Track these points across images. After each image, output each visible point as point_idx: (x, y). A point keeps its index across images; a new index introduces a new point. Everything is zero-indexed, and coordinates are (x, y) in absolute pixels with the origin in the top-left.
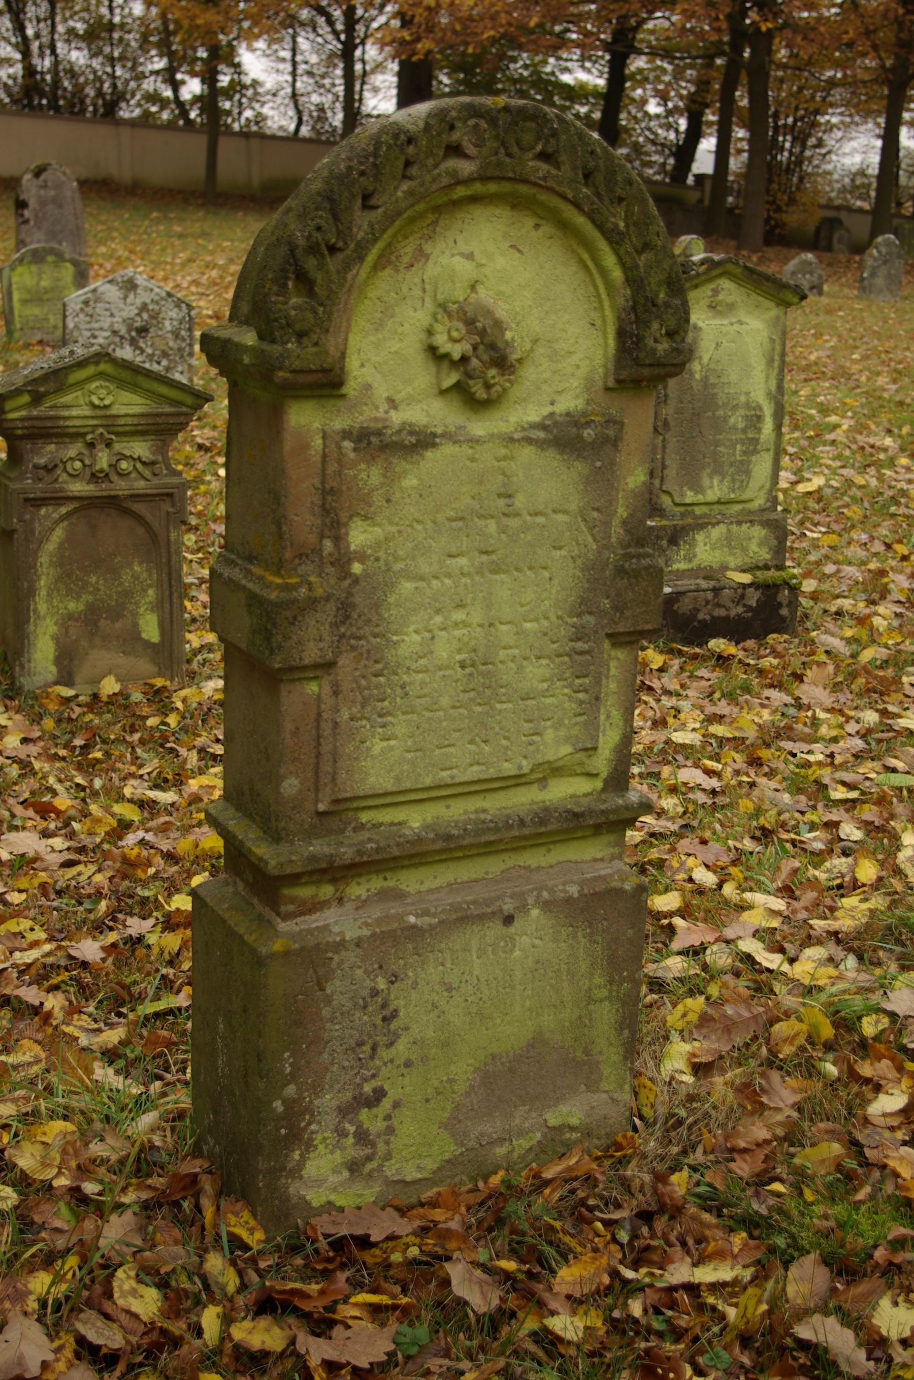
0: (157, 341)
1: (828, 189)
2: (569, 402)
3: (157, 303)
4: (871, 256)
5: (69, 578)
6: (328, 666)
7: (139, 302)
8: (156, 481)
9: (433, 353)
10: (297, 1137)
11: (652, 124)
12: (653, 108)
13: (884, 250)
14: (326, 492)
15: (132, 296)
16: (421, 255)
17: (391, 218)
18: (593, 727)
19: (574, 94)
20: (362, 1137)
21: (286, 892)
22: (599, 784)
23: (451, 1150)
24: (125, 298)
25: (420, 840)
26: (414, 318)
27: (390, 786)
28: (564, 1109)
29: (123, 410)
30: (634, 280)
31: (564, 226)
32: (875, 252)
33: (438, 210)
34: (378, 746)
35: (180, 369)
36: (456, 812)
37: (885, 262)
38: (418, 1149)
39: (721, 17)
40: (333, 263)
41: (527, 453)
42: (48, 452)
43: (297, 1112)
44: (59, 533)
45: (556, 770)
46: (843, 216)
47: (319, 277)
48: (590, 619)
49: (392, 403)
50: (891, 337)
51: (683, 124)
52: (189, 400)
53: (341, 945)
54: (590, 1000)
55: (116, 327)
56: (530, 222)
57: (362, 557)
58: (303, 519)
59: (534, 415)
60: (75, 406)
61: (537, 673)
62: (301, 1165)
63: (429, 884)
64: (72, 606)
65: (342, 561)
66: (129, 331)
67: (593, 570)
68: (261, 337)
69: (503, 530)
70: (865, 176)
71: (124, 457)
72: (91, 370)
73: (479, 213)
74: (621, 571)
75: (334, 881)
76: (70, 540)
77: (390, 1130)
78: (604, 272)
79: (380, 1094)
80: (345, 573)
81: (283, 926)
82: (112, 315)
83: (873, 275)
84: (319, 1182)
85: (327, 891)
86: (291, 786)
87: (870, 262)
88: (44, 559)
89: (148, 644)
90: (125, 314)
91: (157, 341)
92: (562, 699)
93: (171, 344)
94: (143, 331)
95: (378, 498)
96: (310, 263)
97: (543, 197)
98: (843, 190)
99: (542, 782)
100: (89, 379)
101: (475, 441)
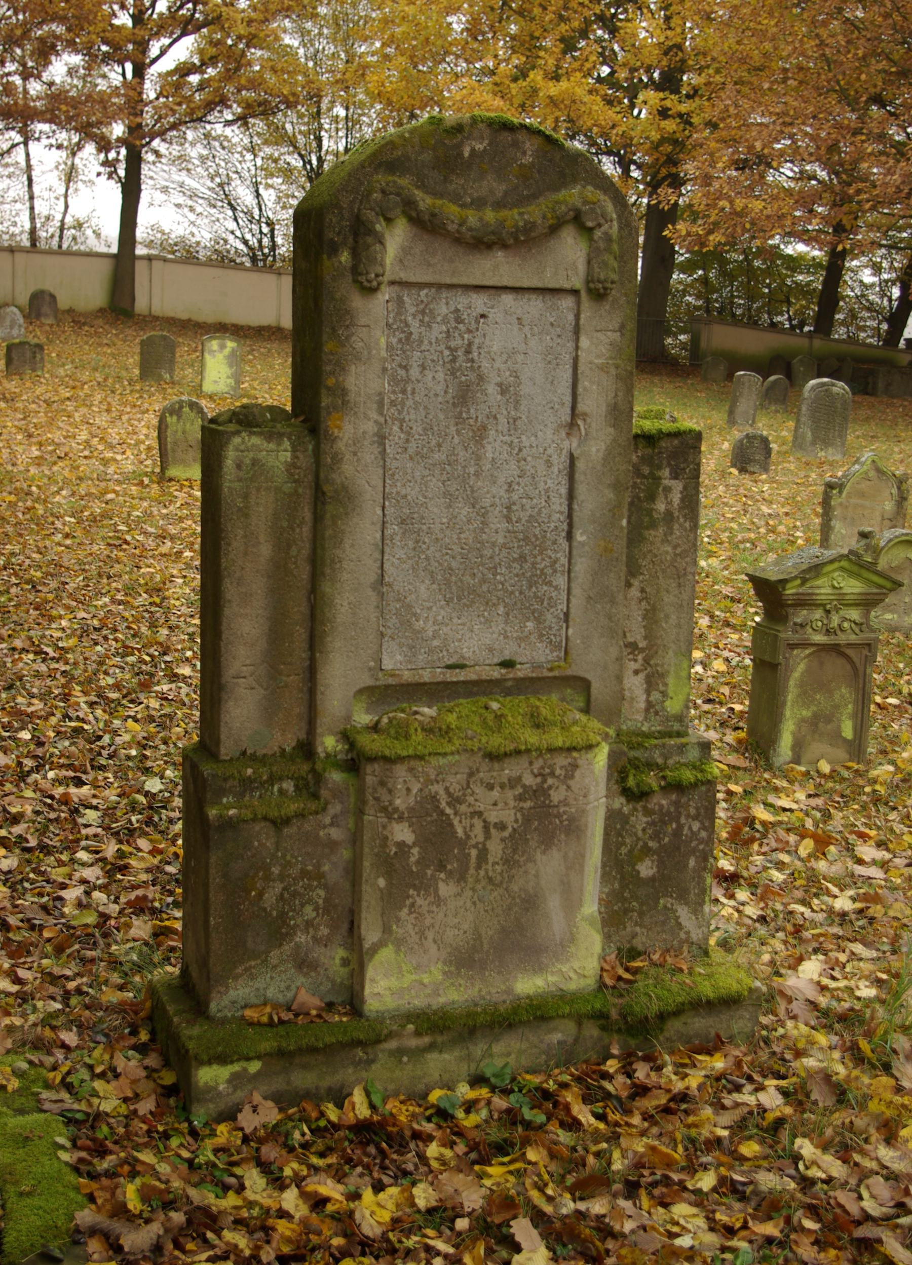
5: (805, 696)
8: (862, 635)
12: (867, 277)
19: (794, 263)
29: (850, 590)
42: (801, 615)
44: (801, 667)
52: (888, 585)
60: (822, 588)
64: (804, 713)
71: (846, 619)
72: (836, 565)
76: (808, 671)
88: (792, 683)
89: (845, 740)
100: (834, 571)
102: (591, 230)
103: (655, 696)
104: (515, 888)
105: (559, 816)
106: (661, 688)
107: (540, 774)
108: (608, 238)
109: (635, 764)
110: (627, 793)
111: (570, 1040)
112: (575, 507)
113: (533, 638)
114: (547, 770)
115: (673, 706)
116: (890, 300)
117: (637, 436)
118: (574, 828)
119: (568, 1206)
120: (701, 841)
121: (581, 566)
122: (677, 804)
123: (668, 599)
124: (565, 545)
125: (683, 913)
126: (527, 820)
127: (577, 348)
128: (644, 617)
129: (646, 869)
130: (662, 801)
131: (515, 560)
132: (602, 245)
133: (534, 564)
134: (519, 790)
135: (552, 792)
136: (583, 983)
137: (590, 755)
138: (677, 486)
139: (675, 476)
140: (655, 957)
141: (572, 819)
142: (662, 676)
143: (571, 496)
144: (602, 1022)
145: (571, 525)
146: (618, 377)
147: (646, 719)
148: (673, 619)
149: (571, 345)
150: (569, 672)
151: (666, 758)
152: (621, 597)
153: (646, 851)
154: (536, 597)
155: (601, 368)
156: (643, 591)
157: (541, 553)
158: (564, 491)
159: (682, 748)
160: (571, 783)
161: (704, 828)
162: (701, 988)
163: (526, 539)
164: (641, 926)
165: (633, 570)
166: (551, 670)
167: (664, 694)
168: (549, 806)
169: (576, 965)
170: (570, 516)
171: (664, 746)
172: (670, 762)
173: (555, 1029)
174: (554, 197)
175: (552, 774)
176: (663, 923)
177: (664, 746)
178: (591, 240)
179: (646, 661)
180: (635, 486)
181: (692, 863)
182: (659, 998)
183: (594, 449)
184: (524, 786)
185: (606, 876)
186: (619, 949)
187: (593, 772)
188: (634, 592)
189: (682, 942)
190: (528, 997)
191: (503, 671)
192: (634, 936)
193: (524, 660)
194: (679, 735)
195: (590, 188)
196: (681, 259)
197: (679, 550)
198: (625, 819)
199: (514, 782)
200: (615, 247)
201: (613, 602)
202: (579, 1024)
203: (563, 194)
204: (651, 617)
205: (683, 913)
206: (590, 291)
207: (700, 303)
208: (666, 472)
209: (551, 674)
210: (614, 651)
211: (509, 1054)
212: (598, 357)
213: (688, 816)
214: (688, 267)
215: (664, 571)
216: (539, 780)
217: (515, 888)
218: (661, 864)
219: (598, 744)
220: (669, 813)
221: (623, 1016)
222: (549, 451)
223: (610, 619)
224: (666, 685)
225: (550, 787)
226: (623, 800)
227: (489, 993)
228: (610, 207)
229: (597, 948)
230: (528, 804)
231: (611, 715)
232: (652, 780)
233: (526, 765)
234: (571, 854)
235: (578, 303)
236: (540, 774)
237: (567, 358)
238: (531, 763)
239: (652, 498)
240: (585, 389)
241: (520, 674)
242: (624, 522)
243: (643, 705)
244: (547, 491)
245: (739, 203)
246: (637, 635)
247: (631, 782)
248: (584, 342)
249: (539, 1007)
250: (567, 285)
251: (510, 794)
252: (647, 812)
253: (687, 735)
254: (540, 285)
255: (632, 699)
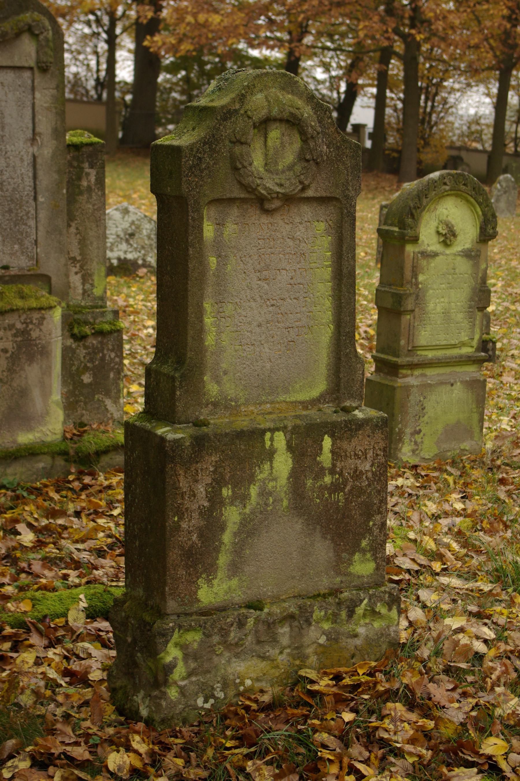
0: (139, 240)
1: (450, 134)
2: (468, 246)
3: (139, 220)
4: (496, 188)
6: (413, 311)
7: (130, 220)
9: (438, 233)
10: (400, 440)
11: (319, 87)
12: (320, 74)
13: (504, 185)
14: (413, 267)
15: (126, 217)
16: (435, 209)
17: (431, 200)
18: (473, 332)
20: (416, 443)
21: (401, 371)
22: (474, 350)
23: (437, 451)
24: (123, 218)
25: (432, 359)
26: (433, 224)
27: (425, 344)
28: (465, 444)
30: (484, 214)
31: (468, 201)
32: (498, 186)
33: (440, 198)
34: (423, 333)
35: (150, 255)
36: (440, 354)
37: (505, 192)
38: (429, 450)
39: (390, 30)
40: (419, 211)
41: (459, 258)
43: (401, 432)
45: (463, 344)
46: (463, 154)
47: (415, 214)
48: (473, 303)
49: (428, 245)
50: (514, 240)
51: (343, 87)
53: (413, 386)
54: (472, 412)
55: (119, 233)
56: (459, 200)
57: (421, 283)
58: (408, 273)
59: (460, 248)
61: (460, 316)
62: (401, 449)
63: (433, 373)
65: (417, 284)
66: (125, 235)
67: (474, 289)
68: (400, 228)
69: (453, 278)
70: (478, 124)
73: (449, 198)
74: (480, 291)
75: (411, 369)
77: (422, 442)
78: (477, 213)
79: (420, 431)
80: (417, 287)
81: (399, 380)
82: (117, 227)
83: (498, 200)
84: (405, 454)
85: (409, 372)
86: (402, 342)
87: (495, 192)
90: (123, 226)
91: (139, 240)
92: (465, 324)
93: (146, 242)
94: (132, 235)
95: (425, 268)
96: (414, 211)
97: (464, 194)
98: (462, 135)
99: (460, 347)
101: (447, 255)
102: (37, 36)
103: (87, 286)
104: (15, 385)
105: (36, 345)
106: (90, 282)
107: (25, 323)
108: (47, 40)
109: (79, 323)
110: (73, 336)
111: (49, 466)
112: (38, 183)
113: (18, 254)
114: (28, 321)
115: (97, 292)
116: (338, 93)
117: (69, 146)
118: (45, 352)
119: (44, 522)
120: (116, 364)
121: (43, 215)
122: (101, 343)
123: (91, 233)
124: (33, 203)
125: (109, 403)
126: (19, 348)
127: (34, 98)
128: (79, 243)
129: (87, 378)
130: (93, 341)
131: (6, 212)
132: (44, 43)
133: (17, 214)
134: (14, 331)
135: (32, 332)
136: (54, 437)
137: (51, 312)
138: (93, 173)
139: (92, 167)
140: (94, 426)
141: (43, 347)
142: (91, 275)
143: (35, 177)
144: (66, 457)
145: (36, 193)
146: (57, 113)
147: (83, 299)
148: (95, 244)
149: (30, 97)
150: (39, 272)
151: (95, 319)
152: (65, 231)
153: (86, 369)
154: (19, 231)
155: (47, 109)
156: (77, 229)
157: (20, 208)
158: (31, 174)
159: (103, 314)
160: (42, 327)
161: (117, 356)
162: (118, 438)
163: (12, 200)
164: (86, 410)
165: (71, 218)
166: (29, 270)
167: (92, 285)
168: (31, 340)
169: (50, 427)
170: (35, 188)
171: (93, 312)
172: (97, 321)
173: (40, 461)
174: (17, 18)
175: (31, 322)
176: (98, 408)
177: (93, 312)
178: (38, 41)
179: (82, 267)
180: (70, 172)
181: (112, 375)
182: (96, 444)
183: (46, 152)
184: (17, 329)
185: (64, 383)
186: (74, 423)
187: (53, 321)
188: (73, 230)
189: (108, 419)
190: (25, 445)
191: (3, 271)
192: (82, 415)
193: (14, 265)
194: (101, 307)
195: (36, 13)
196: (168, 62)
197: (96, 207)
198: (74, 351)
199: (11, 327)
200: (51, 44)
201: (61, 234)
202: (53, 458)
203: (22, 17)
204: (83, 243)
205: (109, 403)
206: (39, 68)
207: (184, 98)
208: (86, 165)
209: (29, 273)
210: (63, 261)
211: (16, 474)
212: (45, 103)
213: (108, 350)
214: (173, 69)
215: (88, 218)
216: (24, 325)
217: (15, 385)
218: (95, 375)
219: (55, 307)
220: (97, 348)
221: (77, 453)
222: (22, 153)
223: (60, 243)
224: (93, 280)
225: (31, 330)
226: (72, 341)
227: (4, 442)
228: (47, 23)
229: (61, 418)
230: (19, 339)
231: (64, 295)
232: (87, 330)
233: (17, 317)
234: (44, 366)
235: (33, 74)
236: (25, 323)
237: (29, 103)
238: (20, 317)
239: (79, 179)
240: (39, 120)
241: (12, 273)
242: (65, 191)
243: (81, 291)
244: (22, 174)
245: (202, 18)
246: (75, 253)
247: (76, 331)
248: (38, 95)
249: (30, 449)
250: (26, 65)
251: (9, 333)
252: (86, 347)
253: (106, 307)
254: (11, 64)
255: (75, 288)
